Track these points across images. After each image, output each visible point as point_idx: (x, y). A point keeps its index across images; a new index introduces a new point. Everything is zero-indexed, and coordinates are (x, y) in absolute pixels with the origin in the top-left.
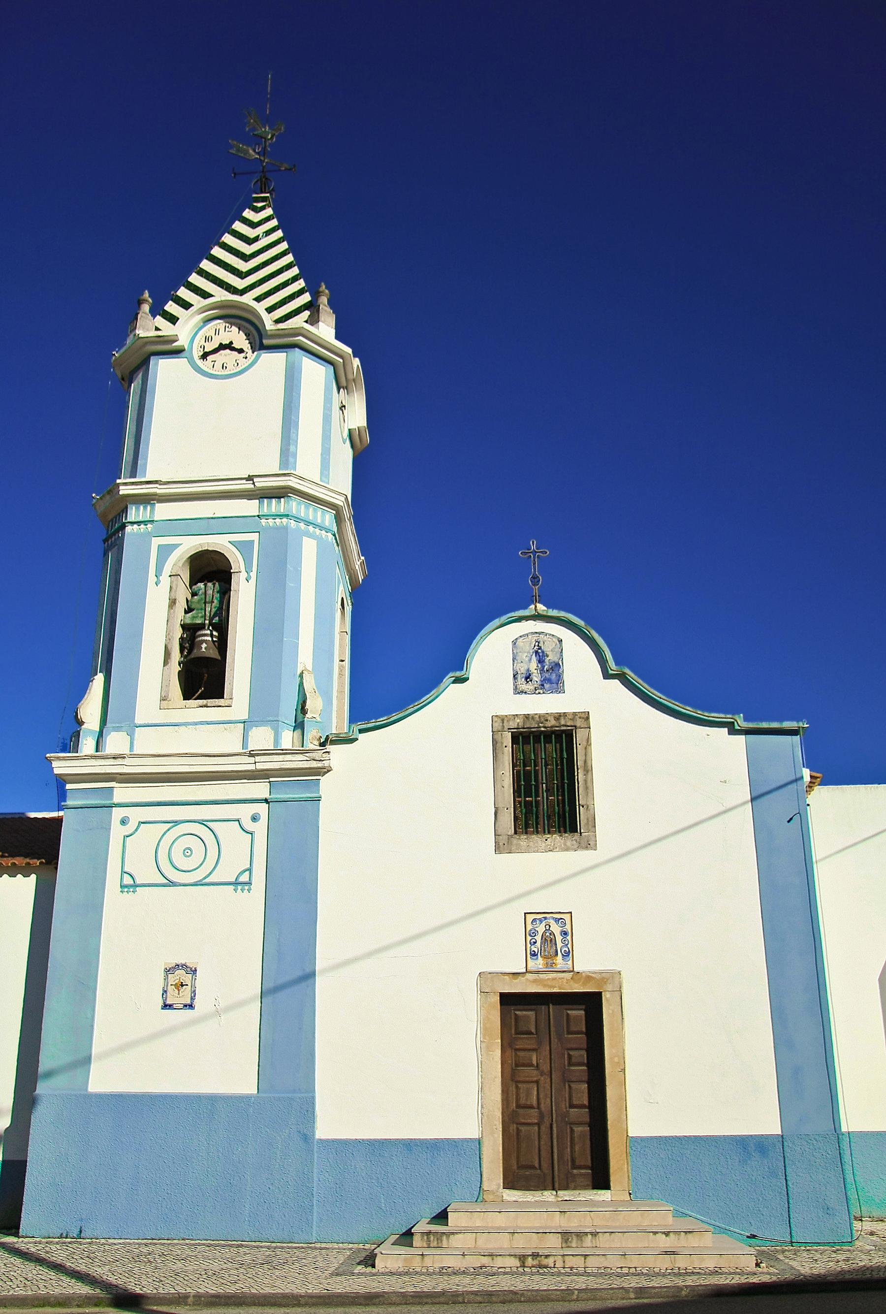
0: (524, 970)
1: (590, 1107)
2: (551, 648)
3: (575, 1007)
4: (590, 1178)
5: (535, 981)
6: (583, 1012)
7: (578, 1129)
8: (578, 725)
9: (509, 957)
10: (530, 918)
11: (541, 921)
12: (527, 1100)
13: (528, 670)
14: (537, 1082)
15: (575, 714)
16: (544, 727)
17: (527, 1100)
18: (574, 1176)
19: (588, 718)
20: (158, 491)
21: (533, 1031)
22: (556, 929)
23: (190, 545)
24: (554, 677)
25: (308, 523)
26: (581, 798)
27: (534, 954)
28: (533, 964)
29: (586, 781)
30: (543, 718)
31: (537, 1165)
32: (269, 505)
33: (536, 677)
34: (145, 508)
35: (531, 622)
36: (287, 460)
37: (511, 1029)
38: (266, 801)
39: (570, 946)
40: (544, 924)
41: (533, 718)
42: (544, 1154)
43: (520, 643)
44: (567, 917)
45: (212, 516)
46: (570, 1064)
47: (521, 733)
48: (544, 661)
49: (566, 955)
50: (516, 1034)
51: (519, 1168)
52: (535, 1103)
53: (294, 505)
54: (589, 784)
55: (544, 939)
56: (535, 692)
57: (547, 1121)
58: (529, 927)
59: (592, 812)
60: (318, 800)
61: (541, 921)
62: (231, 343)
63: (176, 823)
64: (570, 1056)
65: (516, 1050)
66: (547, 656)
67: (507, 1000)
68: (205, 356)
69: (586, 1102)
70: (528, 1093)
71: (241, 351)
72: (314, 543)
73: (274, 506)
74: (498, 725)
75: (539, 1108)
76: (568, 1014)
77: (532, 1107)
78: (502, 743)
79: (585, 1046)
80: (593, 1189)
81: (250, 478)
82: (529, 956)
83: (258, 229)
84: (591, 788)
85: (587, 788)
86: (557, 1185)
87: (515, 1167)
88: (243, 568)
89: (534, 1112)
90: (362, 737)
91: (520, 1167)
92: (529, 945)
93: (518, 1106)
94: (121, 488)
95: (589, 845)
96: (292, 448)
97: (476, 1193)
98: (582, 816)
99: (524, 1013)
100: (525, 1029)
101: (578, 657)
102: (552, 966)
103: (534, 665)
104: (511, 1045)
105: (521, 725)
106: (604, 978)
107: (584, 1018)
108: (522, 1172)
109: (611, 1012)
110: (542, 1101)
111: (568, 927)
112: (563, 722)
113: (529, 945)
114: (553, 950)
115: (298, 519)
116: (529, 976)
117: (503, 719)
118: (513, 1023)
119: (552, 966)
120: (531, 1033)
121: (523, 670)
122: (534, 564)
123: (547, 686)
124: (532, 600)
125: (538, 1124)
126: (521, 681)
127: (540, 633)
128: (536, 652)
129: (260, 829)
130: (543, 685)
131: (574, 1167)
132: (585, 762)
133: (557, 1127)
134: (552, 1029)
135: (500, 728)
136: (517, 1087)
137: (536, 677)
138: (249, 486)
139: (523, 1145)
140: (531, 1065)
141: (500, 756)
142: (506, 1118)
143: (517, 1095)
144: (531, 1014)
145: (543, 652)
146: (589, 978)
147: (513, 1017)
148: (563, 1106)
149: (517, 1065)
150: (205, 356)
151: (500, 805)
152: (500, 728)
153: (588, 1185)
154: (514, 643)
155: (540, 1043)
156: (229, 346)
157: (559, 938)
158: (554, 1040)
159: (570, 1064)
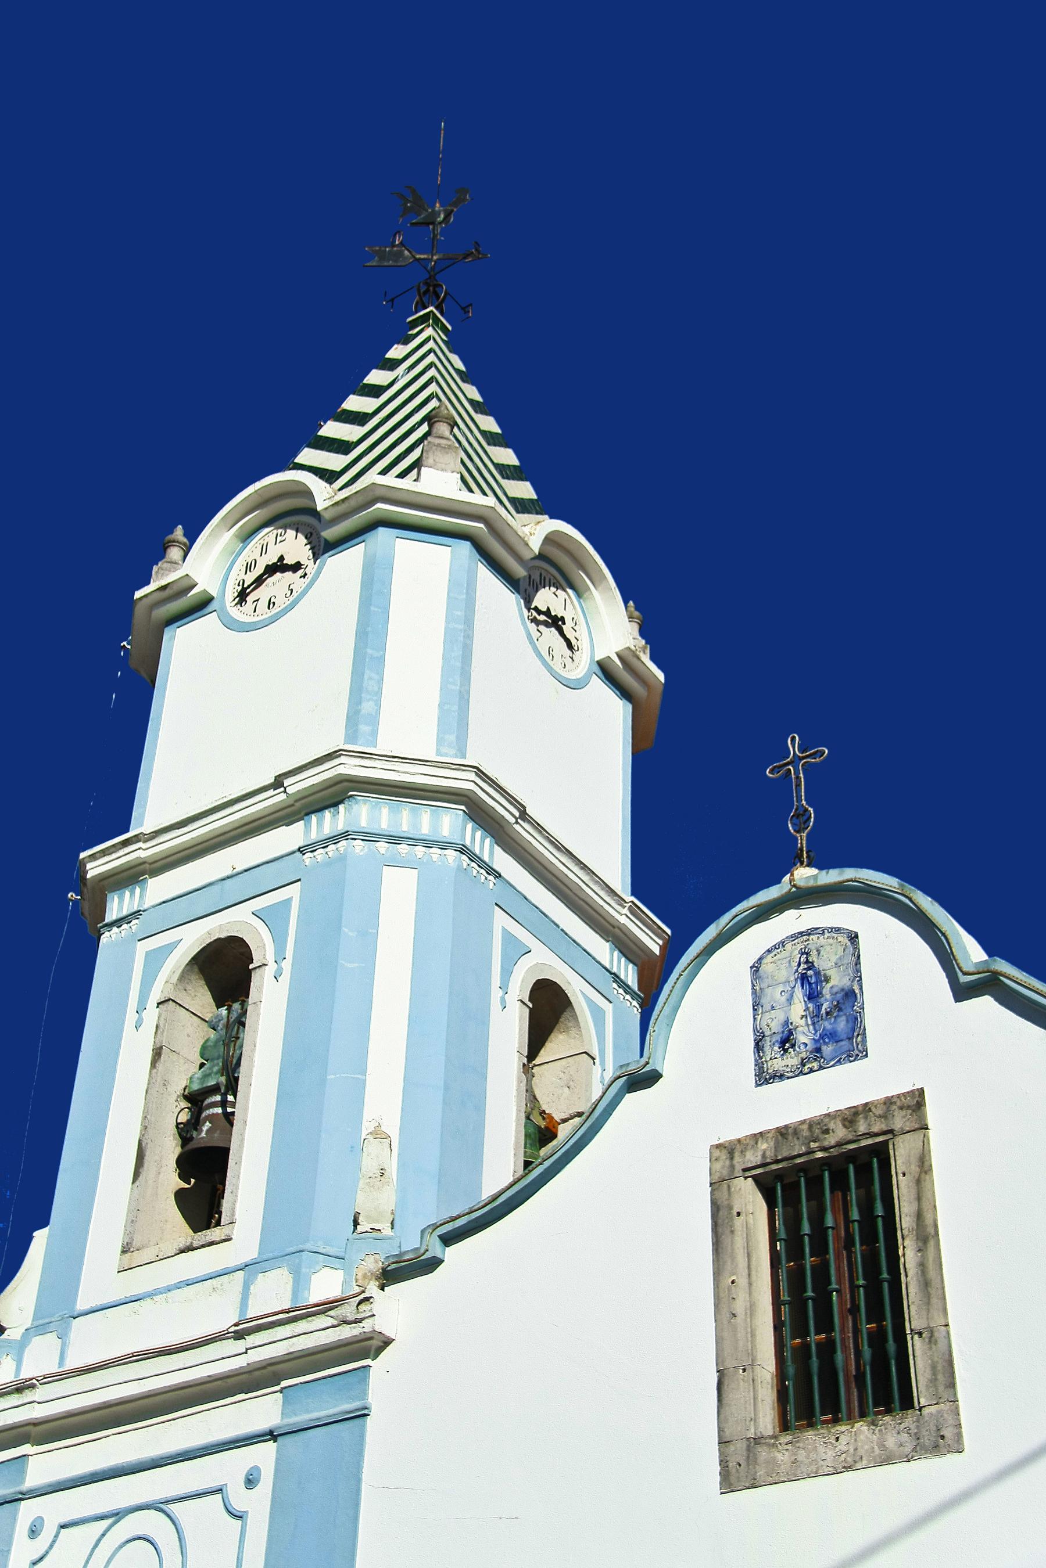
2: (834, 959)
13: (787, 1023)
15: (889, 1102)
16: (824, 1149)
20: (143, 854)
23: (193, 938)
25: (394, 839)
26: (915, 1317)
29: (922, 1266)
30: (818, 1126)
32: (320, 824)
33: (804, 1037)
34: (132, 893)
35: (790, 914)
36: (356, 731)
38: (271, 1435)
43: (767, 967)
45: (229, 872)
48: (819, 994)
53: (363, 812)
54: (932, 1274)
56: (800, 1071)
59: (942, 1345)
60: (361, 1415)
62: (281, 558)
63: (118, 1515)
66: (827, 980)
68: (242, 596)
71: (296, 567)
72: (411, 876)
73: (328, 823)
78: (730, 1208)
81: (278, 783)
83: (422, 364)
84: (935, 1282)
85: (926, 1284)
88: (270, 958)
90: (452, 1253)
94: (89, 866)
95: (943, 1441)
96: (367, 707)
98: (920, 1357)
101: (894, 960)
103: (798, 1009)
105: (770, 1155)
112: (862, 1128)
115: (370, 837)
117: (729, 1149)
121: (776, 1026)
122: (798, 785)
124: (797, 859)
126: (771, 1050)
127: (808, 933)
128: (804, 978)
129: (258, 1503)
130: (818, 1050)
132: (919, 1216)
135: (725, 1172)
137: (804, 1037)
138: (277, 798)
141: (726, 1240)
145: (817, 973)
150: (242, 596)
151: (729, 1363)
154: (756, 969)
156: (279, 567)
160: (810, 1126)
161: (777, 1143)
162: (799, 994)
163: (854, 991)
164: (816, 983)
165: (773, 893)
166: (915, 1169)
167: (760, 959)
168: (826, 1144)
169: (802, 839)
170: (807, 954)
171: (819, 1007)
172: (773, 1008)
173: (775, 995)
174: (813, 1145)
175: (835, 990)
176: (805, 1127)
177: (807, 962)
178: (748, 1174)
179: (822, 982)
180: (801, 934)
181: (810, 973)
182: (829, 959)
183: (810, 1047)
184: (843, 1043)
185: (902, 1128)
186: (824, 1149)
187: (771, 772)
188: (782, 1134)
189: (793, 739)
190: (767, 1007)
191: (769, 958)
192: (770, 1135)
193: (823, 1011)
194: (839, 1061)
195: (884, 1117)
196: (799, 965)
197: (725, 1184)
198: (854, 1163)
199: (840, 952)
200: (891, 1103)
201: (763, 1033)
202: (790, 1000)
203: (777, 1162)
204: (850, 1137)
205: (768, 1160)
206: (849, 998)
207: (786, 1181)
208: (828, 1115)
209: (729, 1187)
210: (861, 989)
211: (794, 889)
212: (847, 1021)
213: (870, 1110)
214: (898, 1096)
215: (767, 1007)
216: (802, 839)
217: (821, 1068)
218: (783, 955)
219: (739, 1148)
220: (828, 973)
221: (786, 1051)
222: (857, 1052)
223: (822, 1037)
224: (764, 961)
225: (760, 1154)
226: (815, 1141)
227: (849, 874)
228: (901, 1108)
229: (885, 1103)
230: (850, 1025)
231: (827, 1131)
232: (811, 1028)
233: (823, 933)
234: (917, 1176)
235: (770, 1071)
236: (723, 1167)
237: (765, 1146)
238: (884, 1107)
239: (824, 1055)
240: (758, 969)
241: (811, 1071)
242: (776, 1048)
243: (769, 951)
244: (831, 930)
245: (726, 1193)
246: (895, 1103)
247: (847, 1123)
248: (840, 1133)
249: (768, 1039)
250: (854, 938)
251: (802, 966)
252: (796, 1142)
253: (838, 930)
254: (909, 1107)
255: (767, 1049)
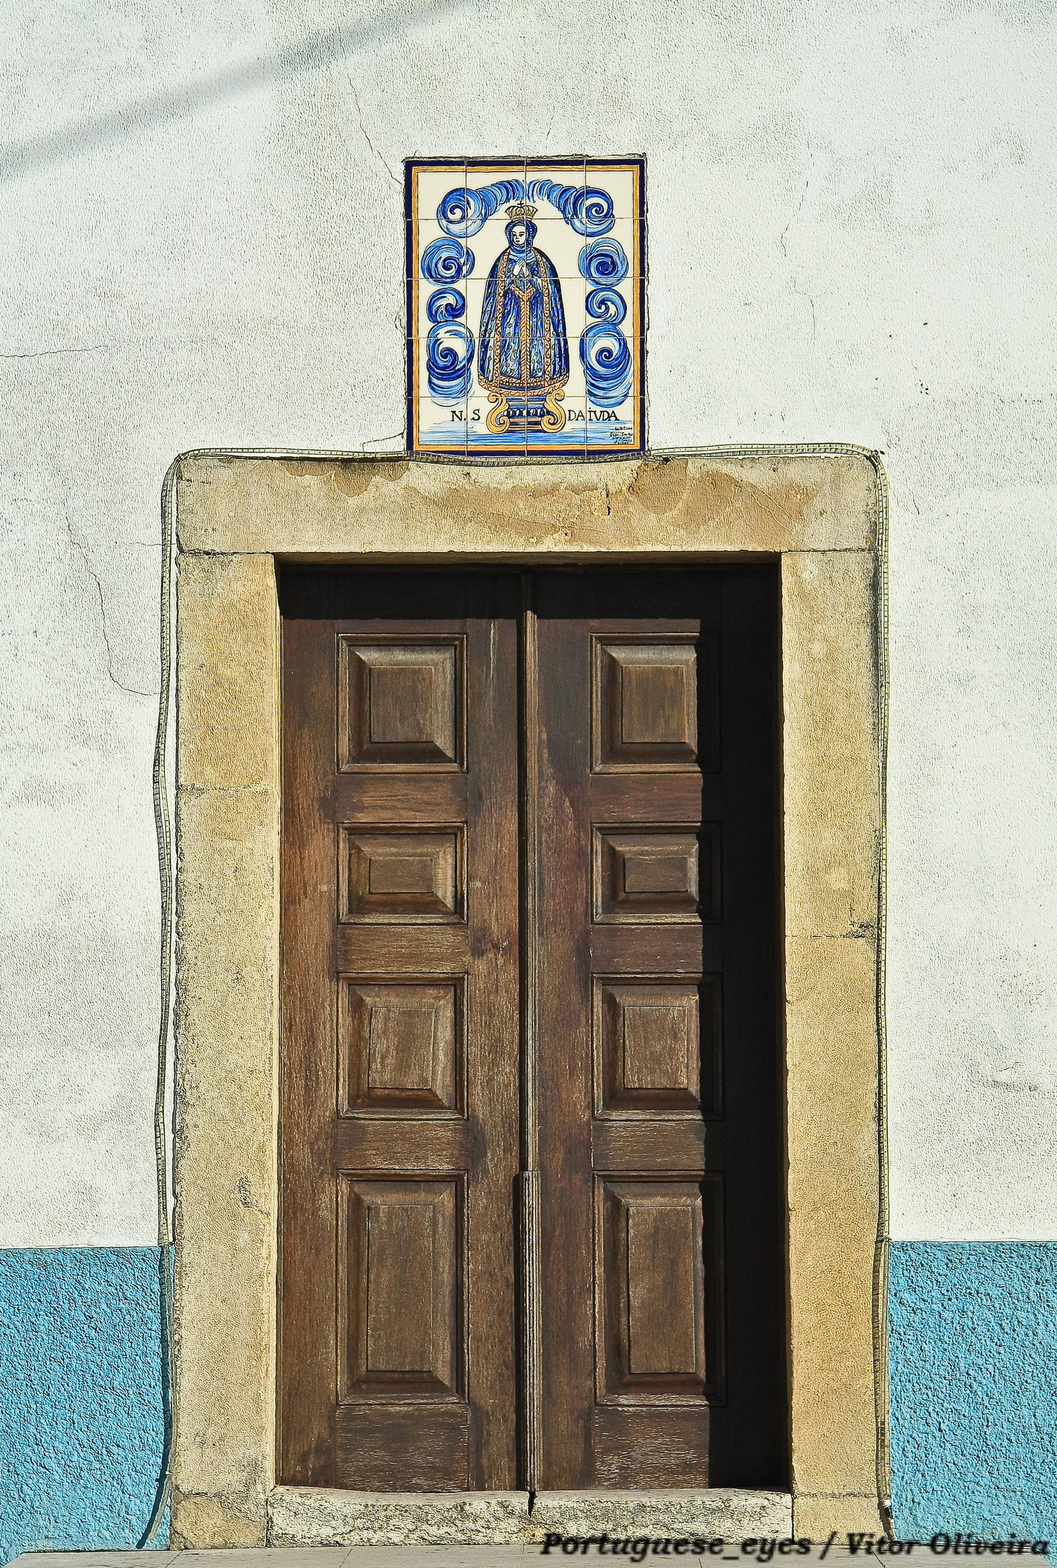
0: (399, 445)
1: (709, 1103)
3: (647, 626)
4: (702, 1434)
5: (448, 503)
6: (688, 656)
7: (645, 1206)
9: (318, 388)
10: (433, 187)
11: (487, 200)
12: (402, 1066)
14: (455, 984)
17: (402, 1066)
18: (616, 1420)
21: (443, 741)
22: (561, 242)
27: (447, 369)
28: (435, 418)
31: (444, 1373)
32: (653, 1082)
37: (333, 735)
39: (627, 328)
40: (501, 218)
42: (480, 1318)
44: (619, 185)
46: (615, 900)
49: (619, 367)
50: (360, 754)
51: (356, 1384)
52: (441, 1084)
55: (501, 296)
57: (497, 1165)
58: (429, 232)
61: (487, 200)
64: (615, 864)
65: (358, 832)
67: (312, 588)
69: (690, 1081)
70: (410, 1041)
75: (459, 1102)
76: (612, 666)
77: (425, 1101)
79: (695, 817)
80: (713, 1484)
82: (422, 375)
86: (535, 1467)
87: (339, 1382)
89: (439, 1127)
91: (364, 1382)
92: (424, 325)
93: (363, 1097)
97: (141, 1507)
99: (401, 656)
100: (402, 733)
102: (535, 427)
104: (331, 809)
106: (792, 487)
107: (691, 683)
108: (372, 1405)
109: (818, 649)
110: (478, 1074)
111: (623, 233)
113: (424, 325)
114: (544, 349)
116: (424, 477)
118: (345, 706)
119: (535, 427)
120: (435, 755)
125: (457, 1182)
131: (622, 1378)
133: (545, 1193)
134: (535, 733)
136: (357, 1007)
139: (382, 1279)
140: (428, 904)
142: (304, 1156)
143: (359, 1042)
144: (437, 664)
146: (714, 474)
147: (345, 677)
148: (579, 1097)
149: (359, 905)
153: (687, 1468)
155: (471, 799)
157: (575, 290)
158: (543, 790)
159: (617, 898)
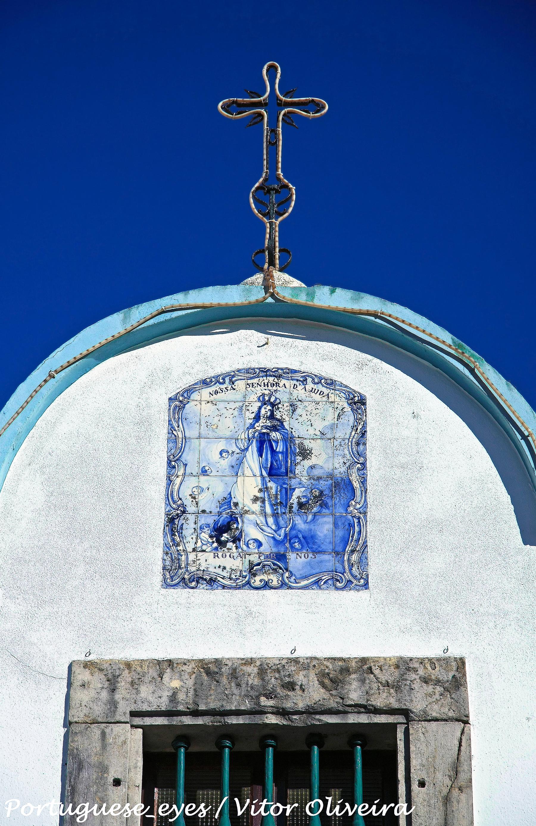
8: (417, 705)
13: (227, 501)
15: (404, 665)
16: (282, 712)
19: (457, 684)
24: (325, 528)
30: (279, 675)
41: (234, 674)
43: (200, 407)
47: (184, 736)
48: (289, 472)
56: (246, 580)
66: (305, 454)
74: (91, 699)
78: (104, 769)
103: (248, 487)
105: (185, 700)
112: (355, 695)
117: (112, 677)
122: (273, 144)
123: (297, 561)
127: (279, 374)
128: (263, 442)
130: (281, 557)
135: (99, 710)
145: (288, 439)
152: (99, 710)
154: (179, 403)
160: (262, 672)
161: (198, 684)
162: (253, 461)
163: (350, 482)
164: (285, 453)
165: (230, 295)
166: (442, 779)
167: (189, 391)
168: (288, 705)
169: (273, 229)
170: (273, 405)
171: (288, 492)
172: (204, 472)
173: (209, 451)
174: (264, 701)
175: (316, 472)
176: (253, 670)
177: (272, 417)
178: (138, 721)
179: (294, 454)
180: (266, 372)
181: (275, 435)
182: (311, 422)
183: (266, 548)
184: (326, 557)
185: (425, 712)
186: (282, 712)
187: (319, 107)
188: (208, 673)
189: (272, 70)
190: (193, 468)
191: (205, 392)
192: (188, 669)
193: (294, 500)
194: (317, 582)
195: (396, 686)
196: (257, 418)
197: (96, 731)
198: (319, 747)
199: (331, 417)
200: (408, 669)
201: (183, 505)
202: (236, 468)
203: (196, 713)
204: (332, 704)
205: (181, 708)
206: (342, 492)
207: (194, 749)
208: (296, 661)
209: (103, 734)
210: (363, 482)
211: (270, 300)
212: (336, 525)
213: (370, 670)
214: (422, 661)
215: (193, 468)
216: (273, 229)
217: (283, 585)
218: (230, 395)
219: (126, 676)
220: (307, 444)
221: (222, 544)
222: (348, 576)
223: (289, 538)
224: (195, 396)
225: (166, 694)
226: (268, 696)
227: (369, 303)
228: (426, 680)
229: (397, 667)
230: (340, 533)
231: (291, 686)
232: (271, 520)
233: (304, 381)
234: (445, 791)
235: (193, 569)
236: (95, 700)
237: (176, 684)
238: (397, 673)
239: (291, 567)
240: (181, 407)
241: (266, 586)
242: (205, 536)
243: (205, 383)
244: (319, 380)
245: (98, 745)
246: (415, 670)
247: (327, 681)
248: (316, 694)
249: (192, 518)
250: (358, 403)
251: (262, 422)
252: (236, 691)
253: (331, 383)
254: (438, 682)
255: (188, 531)
